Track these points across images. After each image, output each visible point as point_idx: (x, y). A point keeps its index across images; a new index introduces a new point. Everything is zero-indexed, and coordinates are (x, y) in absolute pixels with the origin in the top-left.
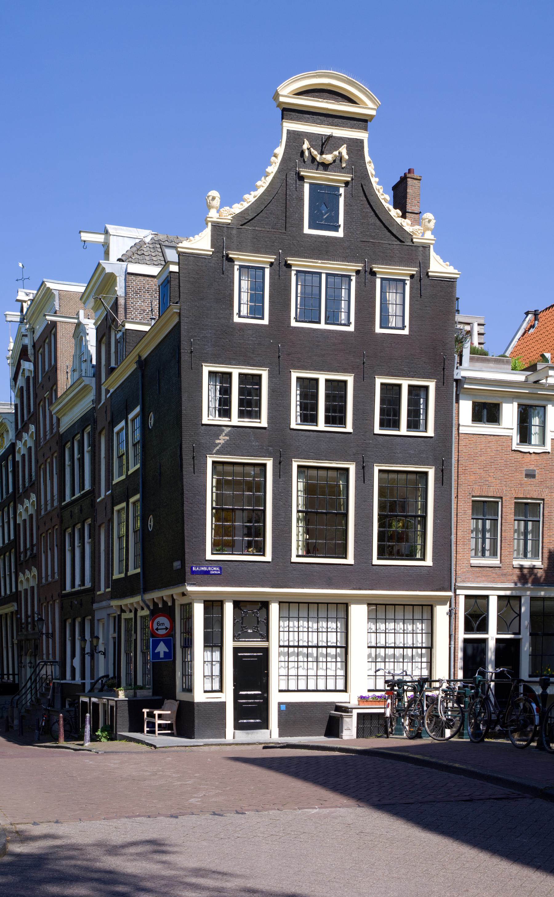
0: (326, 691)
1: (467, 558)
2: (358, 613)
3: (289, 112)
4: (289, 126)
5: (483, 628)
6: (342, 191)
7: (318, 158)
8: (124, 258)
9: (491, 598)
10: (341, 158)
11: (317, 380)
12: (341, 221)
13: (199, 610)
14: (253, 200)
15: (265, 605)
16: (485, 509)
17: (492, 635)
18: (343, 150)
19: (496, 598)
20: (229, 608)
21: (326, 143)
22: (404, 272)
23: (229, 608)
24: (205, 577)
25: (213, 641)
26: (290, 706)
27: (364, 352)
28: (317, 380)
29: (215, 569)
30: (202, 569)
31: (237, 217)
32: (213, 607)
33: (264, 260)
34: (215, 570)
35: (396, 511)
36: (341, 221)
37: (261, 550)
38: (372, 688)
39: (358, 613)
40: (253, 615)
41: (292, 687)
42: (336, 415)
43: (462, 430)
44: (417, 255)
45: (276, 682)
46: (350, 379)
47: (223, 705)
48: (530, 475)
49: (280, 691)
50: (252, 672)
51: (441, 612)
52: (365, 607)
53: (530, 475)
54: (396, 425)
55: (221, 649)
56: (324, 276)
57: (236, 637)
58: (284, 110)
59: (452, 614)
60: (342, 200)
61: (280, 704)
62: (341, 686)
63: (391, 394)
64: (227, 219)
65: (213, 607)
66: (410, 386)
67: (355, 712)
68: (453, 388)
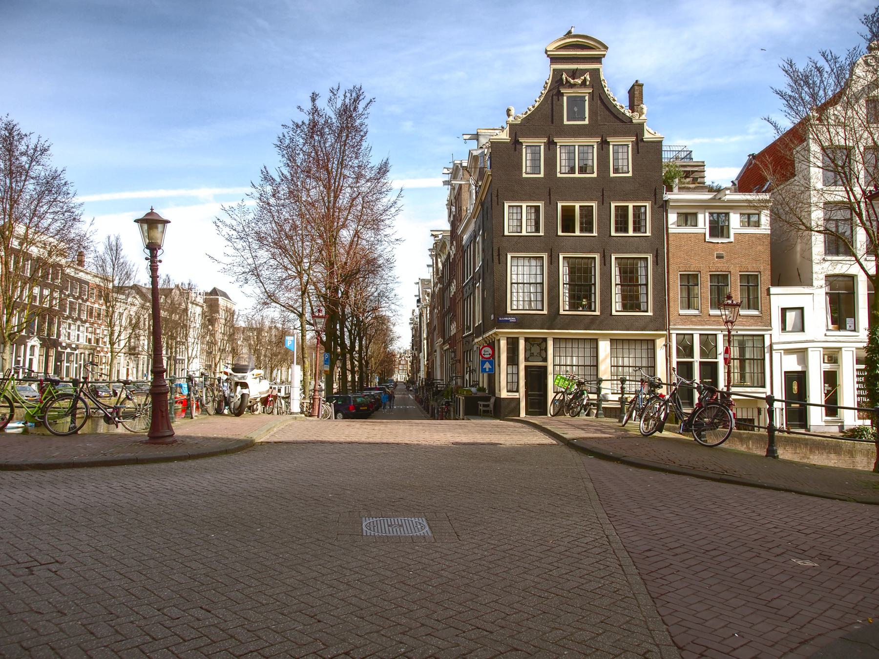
1: (677, 309)
2: (604, 347)
5: (691, 355)
6: (587, 98)
7: (572, 81)
12: (587, 115)
13: (503, 343)
15: (545, 340)
16: (690, 280)
17: (697, 358)
20: (522, 343)
21: (574, 74)
22: (629, 141)
23: (522, 343)
25: (513, 360)
27: (604, 188)
32: (513, 344)
33: (541, 142)
36: (587, 115)
39: (604, 347)
40: (537, 346)
43: (670, 231)
44: (638, 131)
46: (594, 204)
47: (518, 400)
48: (720, 257)
50: (537, 379)
51: (660, 343)
52: (609, 343)
53: (720, 257)
54: (626, 231)
55: (518, 365)
57: (526, 360)
58: (551, 59)
59: (668, 347)
63: (622, 213)
65: (513, 344)
68: (662, 207)
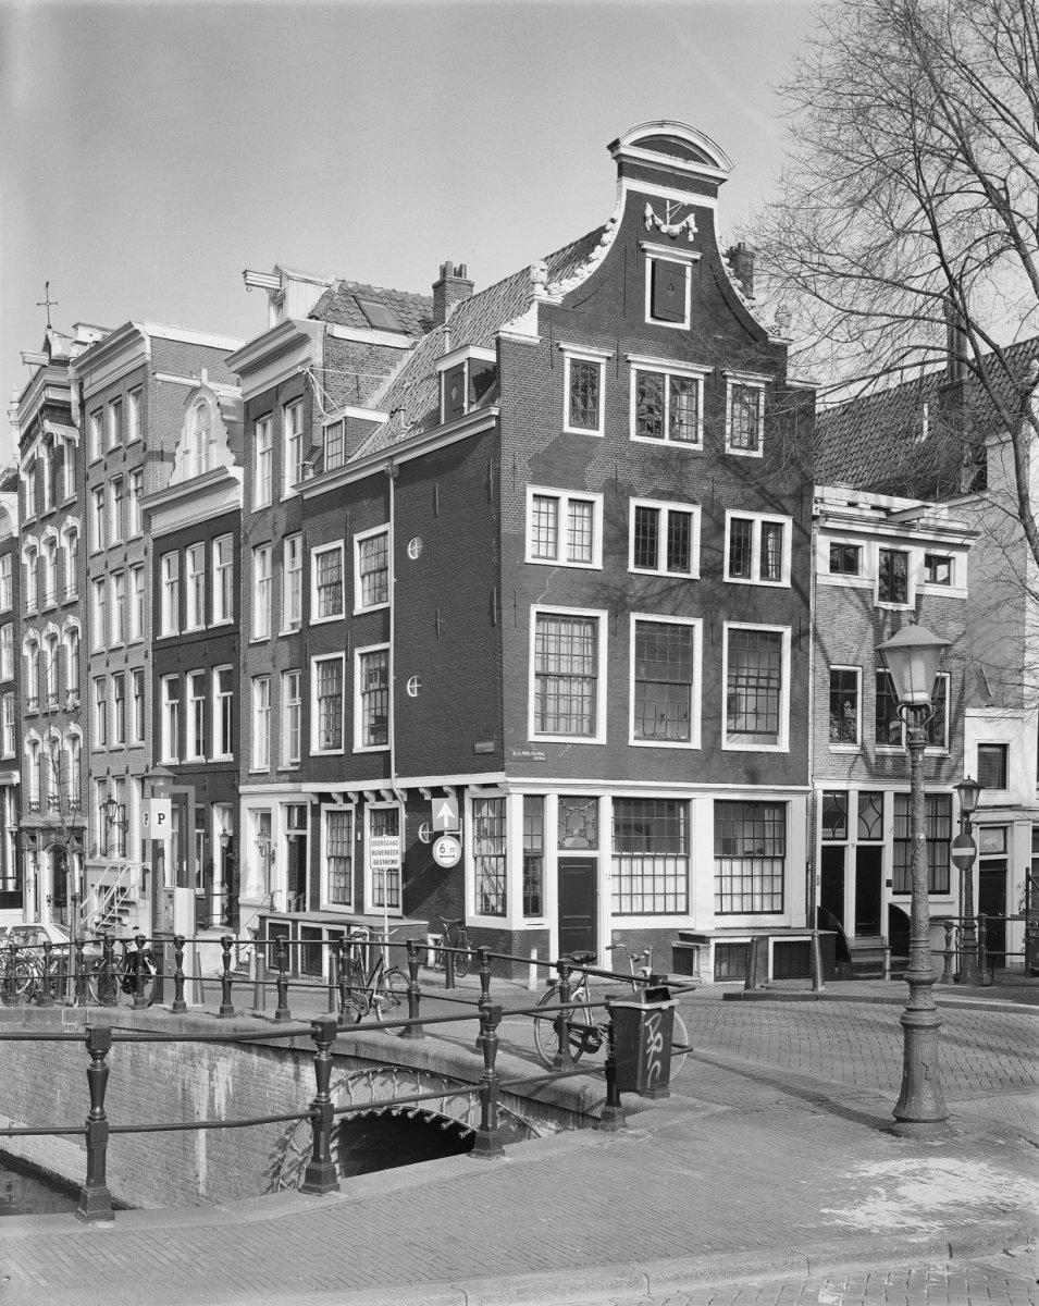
0: (631, 914)
3: (626, 168)
4: (631, 184)
7: (664, 229)
8: (317, 314)
9: (886, 794)
10: (688, 229)
11: (656, 511)
14: (587, 276)
18: (691, 219)
19: (521, 799)
22: (757, 380)
24: (529, 767)
26: (626, 934)
28: (656, 511)
29: (539, 753)
30: (524, 753)
31: (570, 296)
32: (534, 803)
33: (596, 354)
34: (539, 755)
35: (677, 678)
37: (773, 734)
38: (719, 910)
41: (626, 909)
42: (679, 557)
43: (820, 580)
44: (773, 358)
45: (606, 903)
49: (614, 915)
54: (653, 563)
56: (667, 378)
60: (688, 283)
61: (613, 931)
62: (682, 908)
64: (557, 300)
65: (534, 803)
66: (671, 512)
67: (713, 942)
